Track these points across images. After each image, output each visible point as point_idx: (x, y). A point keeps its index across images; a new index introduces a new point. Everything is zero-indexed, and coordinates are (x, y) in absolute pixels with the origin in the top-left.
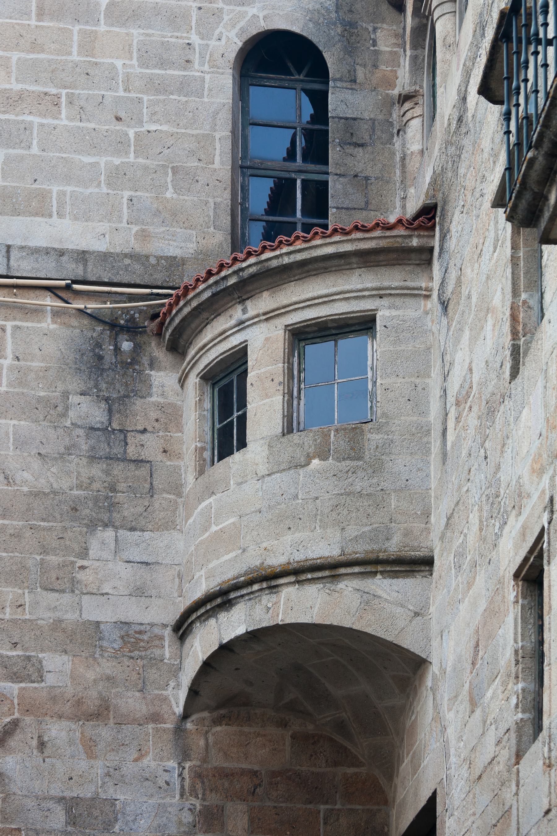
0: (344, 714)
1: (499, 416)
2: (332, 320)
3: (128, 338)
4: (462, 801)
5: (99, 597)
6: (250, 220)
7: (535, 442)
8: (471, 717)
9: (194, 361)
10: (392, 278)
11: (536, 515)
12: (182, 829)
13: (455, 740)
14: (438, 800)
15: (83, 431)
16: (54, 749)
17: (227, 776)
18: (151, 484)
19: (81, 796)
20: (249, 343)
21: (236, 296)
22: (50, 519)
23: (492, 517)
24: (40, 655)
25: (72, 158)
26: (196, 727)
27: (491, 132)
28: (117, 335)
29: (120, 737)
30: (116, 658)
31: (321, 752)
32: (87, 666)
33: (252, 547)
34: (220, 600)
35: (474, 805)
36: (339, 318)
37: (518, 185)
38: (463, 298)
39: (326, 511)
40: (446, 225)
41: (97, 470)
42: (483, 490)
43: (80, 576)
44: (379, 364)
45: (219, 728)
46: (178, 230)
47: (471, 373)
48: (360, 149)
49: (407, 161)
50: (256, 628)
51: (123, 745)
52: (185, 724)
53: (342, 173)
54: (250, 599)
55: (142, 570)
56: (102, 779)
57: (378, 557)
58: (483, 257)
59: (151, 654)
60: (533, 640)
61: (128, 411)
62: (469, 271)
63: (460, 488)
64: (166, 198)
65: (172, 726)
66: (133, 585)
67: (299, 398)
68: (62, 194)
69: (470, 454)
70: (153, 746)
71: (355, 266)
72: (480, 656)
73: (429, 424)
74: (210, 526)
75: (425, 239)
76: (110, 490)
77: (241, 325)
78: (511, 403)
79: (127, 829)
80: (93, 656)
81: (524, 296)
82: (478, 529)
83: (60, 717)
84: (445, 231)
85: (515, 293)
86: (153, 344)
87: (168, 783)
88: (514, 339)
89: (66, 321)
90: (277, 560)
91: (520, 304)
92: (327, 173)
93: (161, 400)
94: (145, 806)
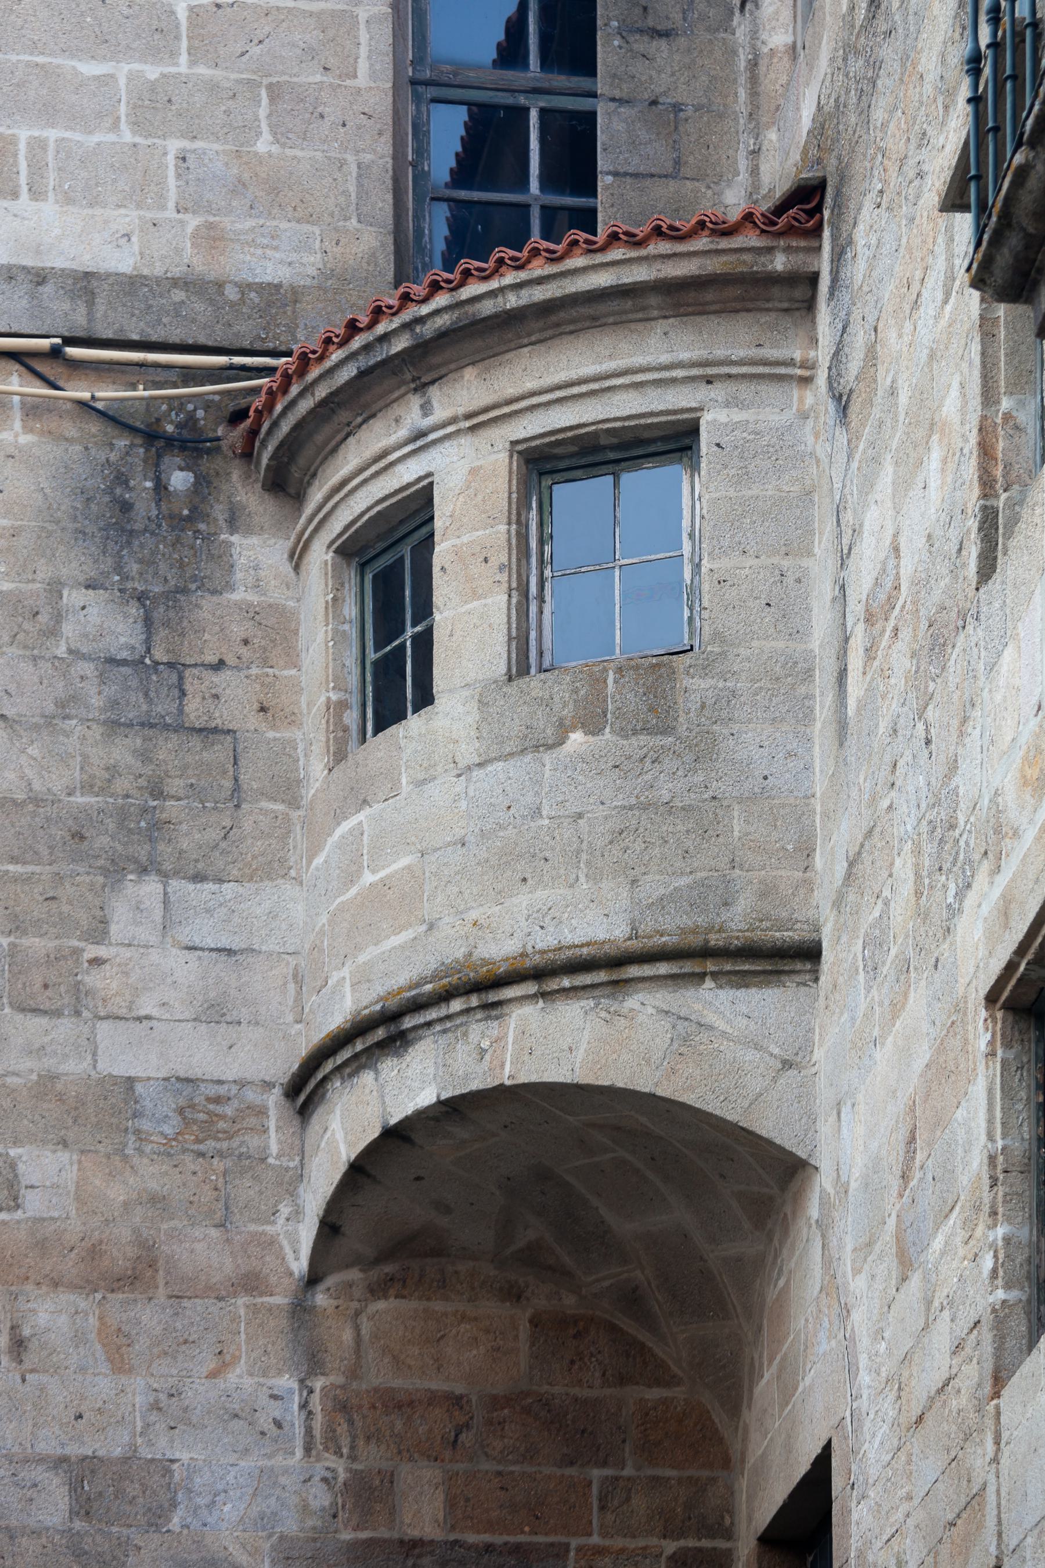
0: (638, 1272)
1: (954, 656)
2: (608, 430)
3: (183, 464)
4: (884, 1467)
5: (131, 1024)
6: (433, 199)
7: (1027, 720)
8: (902, 1291)
9: (321, 515)
10: (731, 340)
11: (1030, 876)
12: (310, 1523)
13: (868, 1342)
14: (834, 1464)
15: (92, 666)
16: (44, 1353)
17: (400, 1407)
18: (236, 780)
19: (100, 1453)
20: (436, 479)
21: (408, 376)
22: (28, 856)
23: (940, 869)
24: (12, 1152)
25: (58, 66)
26: (335, 1303)
27: (940, 39)
28: (159, 456)
29: (179, 1325)
30: (169, 1155)
31: (592, 1355)
32: (110, 1174)
33: (447, 919)
34: (382, 1032)
35: (909, 1478)
36: (624, 427)
37: (994, 219)
38: (880, 393)
39: (599, 843)
40: (844, 227)
41: (122, 752)
42: (923, 810)
43: (93, 979)
44: (707, 528)
45: (381, 1305)
46: (284, 225)
47: (898, 557)
48: (663, 43)
49: (762, 68)
50: (457, 1092)
51: (186, 1342)
52: (313, 1296)
53: (624, 96)
54: (445, 1031)
55: (220, 966)
56: (143, 1418)
57: (707, 941)
58: (922, 310)
59: (240, 1146)
60: (1026, 1136)
61: (185, 623)
62: (893, 335)
63: (873, 800)
64: (256, 154)
65: (286, 1301)
66: (201, 998)
67: (541, 599)
68: (38, 145)
69: (895, 731)
70: (247, 1343)
71: (655, 313)
72: (918, 1163)
73: (809, 656)
74: (359, 873)
75: (801, 256)
76: (151, 794)
77: (420, 440)
78: (980, 633)
79: (196, 1524)
80: (121, 1151)
81: (1006, 404)
82: (912, 892)
83: (56, 1284)
84: (842, 241)
85: (989, 396)
86: (235, 476)
87: (278, 1424)
88: (985, 496)
89: (53, 426)
90: (499, 949)
91: (999, 421)
92: (594, 95)
93: (253, 598)
94: (233, 1473)
